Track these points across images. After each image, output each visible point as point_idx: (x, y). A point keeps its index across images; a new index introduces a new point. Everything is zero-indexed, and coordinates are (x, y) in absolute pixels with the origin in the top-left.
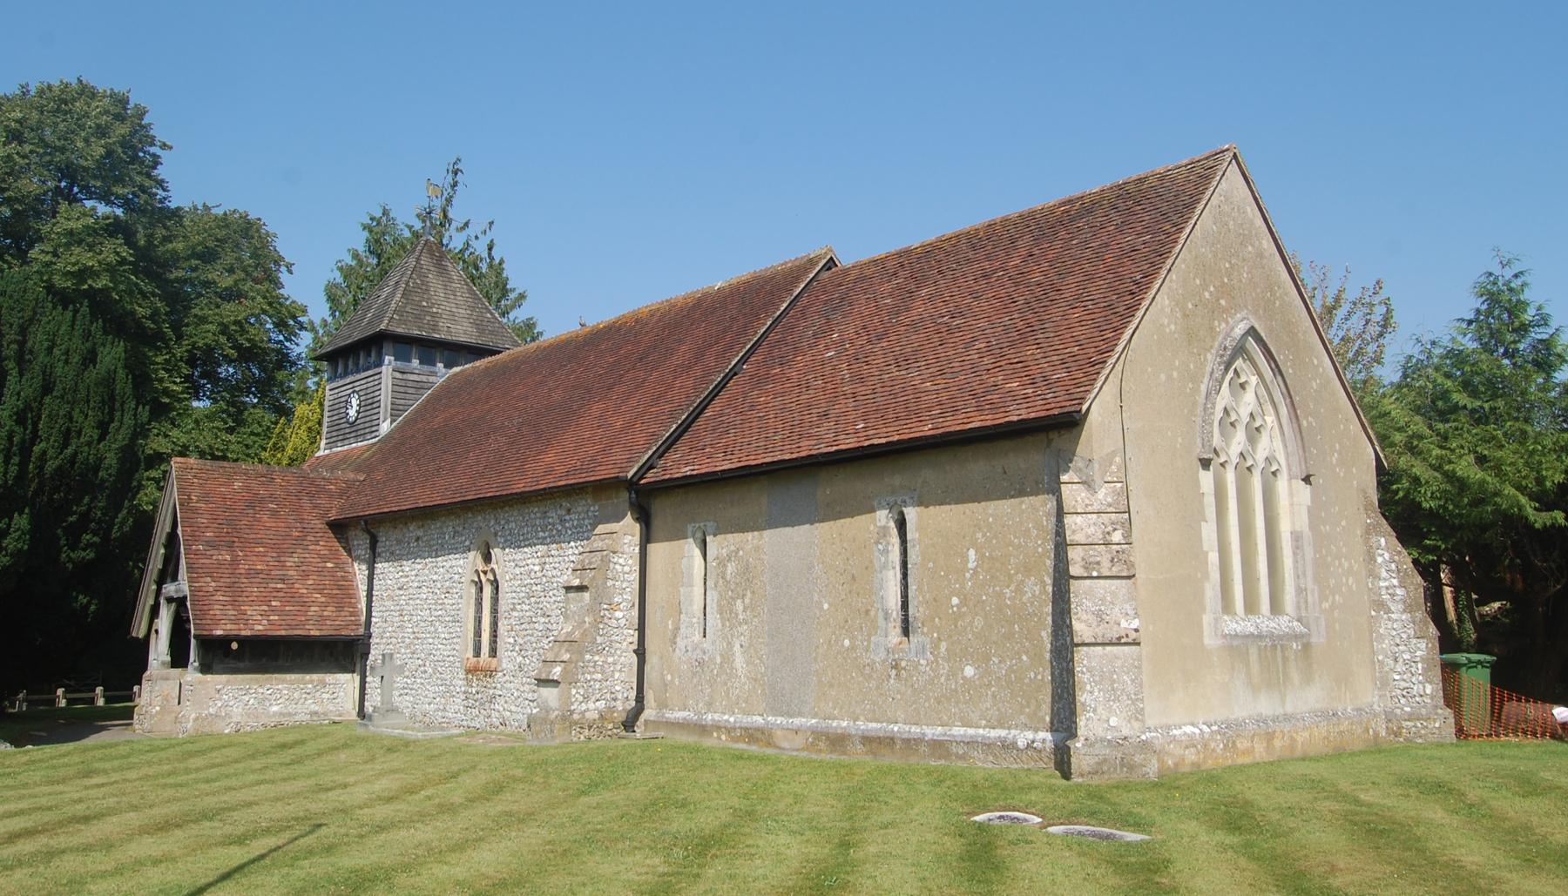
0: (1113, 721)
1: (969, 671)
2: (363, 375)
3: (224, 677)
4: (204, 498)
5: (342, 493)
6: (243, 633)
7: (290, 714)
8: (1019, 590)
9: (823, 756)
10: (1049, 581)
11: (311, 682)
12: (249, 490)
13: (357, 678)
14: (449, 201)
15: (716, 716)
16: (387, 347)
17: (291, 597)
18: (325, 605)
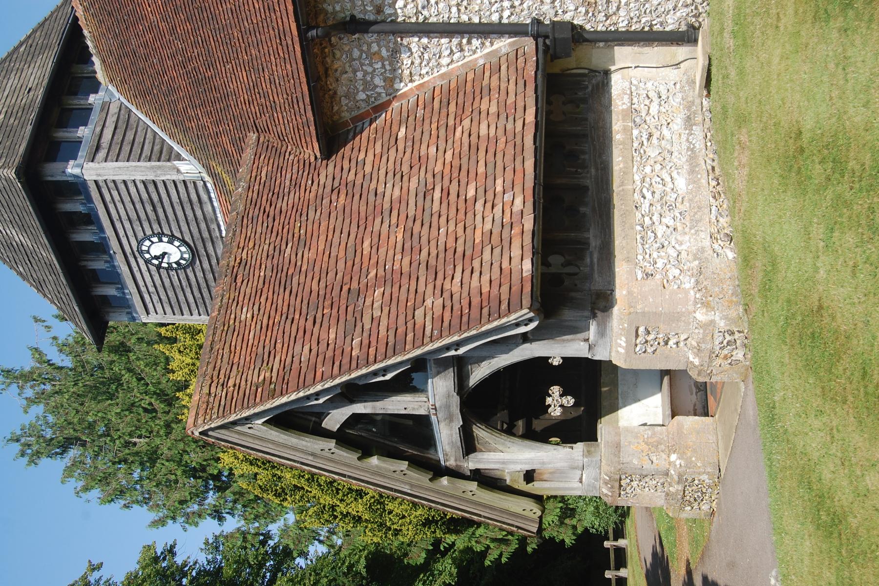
2: (109, 232)
3: (621, 269)
6: (529, 223)
13: (623, 55)
17: (459, 171)
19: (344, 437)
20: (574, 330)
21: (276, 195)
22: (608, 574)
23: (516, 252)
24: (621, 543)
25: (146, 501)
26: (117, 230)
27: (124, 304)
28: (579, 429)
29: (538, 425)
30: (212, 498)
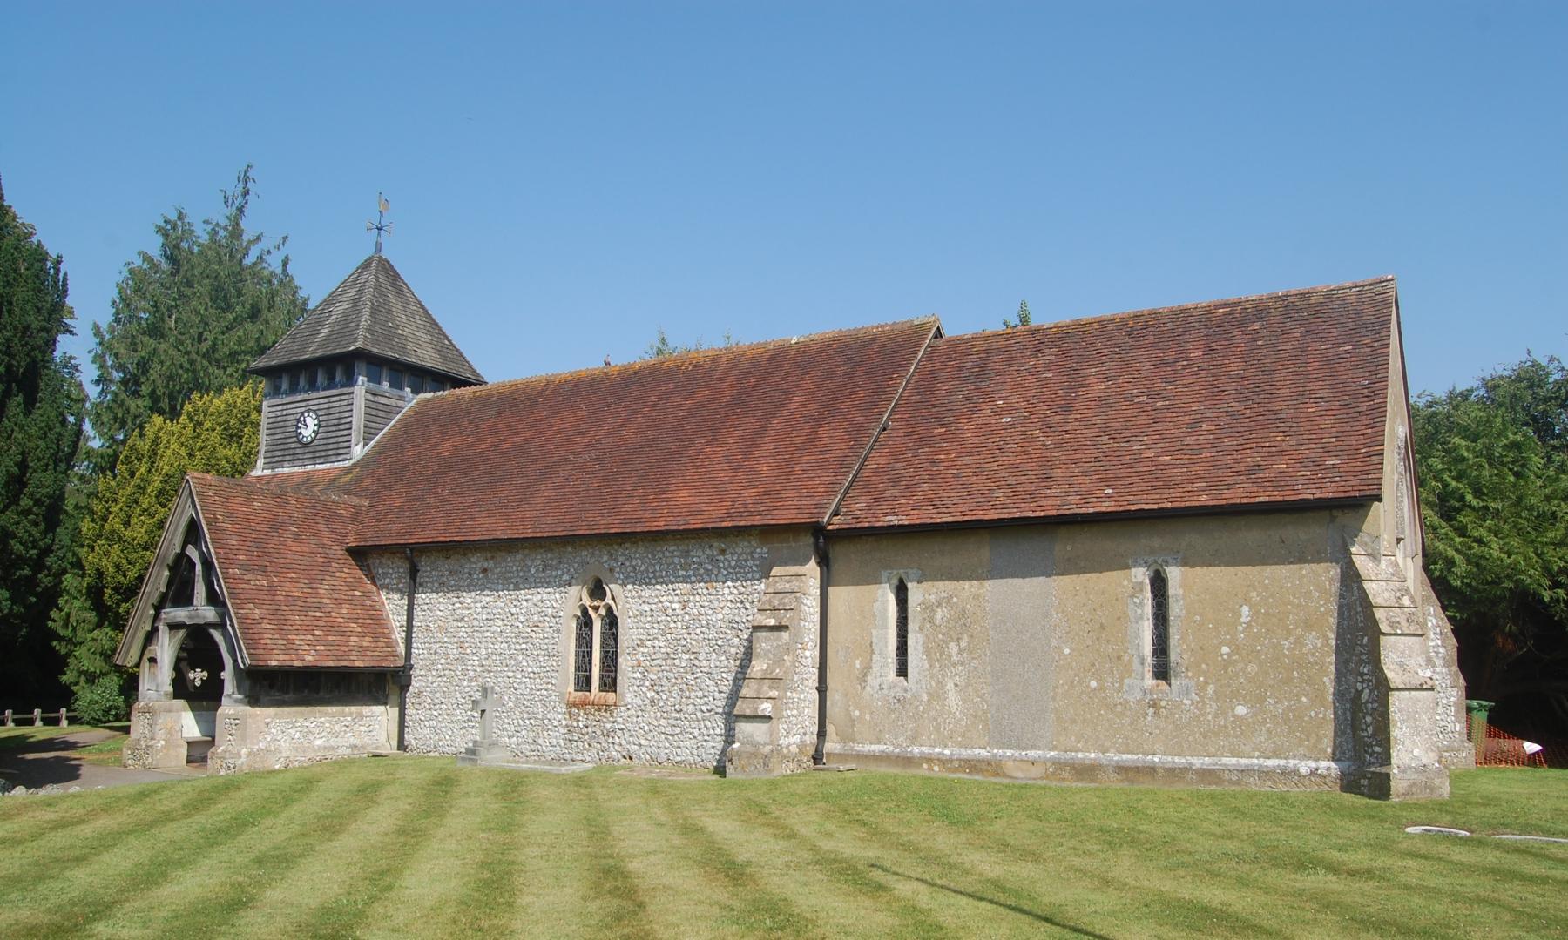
0: (1416, 752)
1: (1241, 710)
2: (322, 394)
3: (272, 710)
4: (229, 517)
5: (353, 519)
6: (296, 664)
7: (333, 748)
8: (1299, 642)
9: (1067, 784)
10: (1332, 636)
11: (350, 714)
12: (269, 512)
13: (394, 712)
14: (241, 210)
15: (925, 749)
16: (360, 367)
17: (331, 626)
18: (362, 636)
19: (182, 556)
20: (239, 689)
21: (327, 520)
22: (37, 712)
23: (281, 657)
24: (64, 723)
25: (117, 320)
26: (322, 398)
27: (276, 391)
28: (181, 689)
29: (184, 665)
30: (117, 376)
